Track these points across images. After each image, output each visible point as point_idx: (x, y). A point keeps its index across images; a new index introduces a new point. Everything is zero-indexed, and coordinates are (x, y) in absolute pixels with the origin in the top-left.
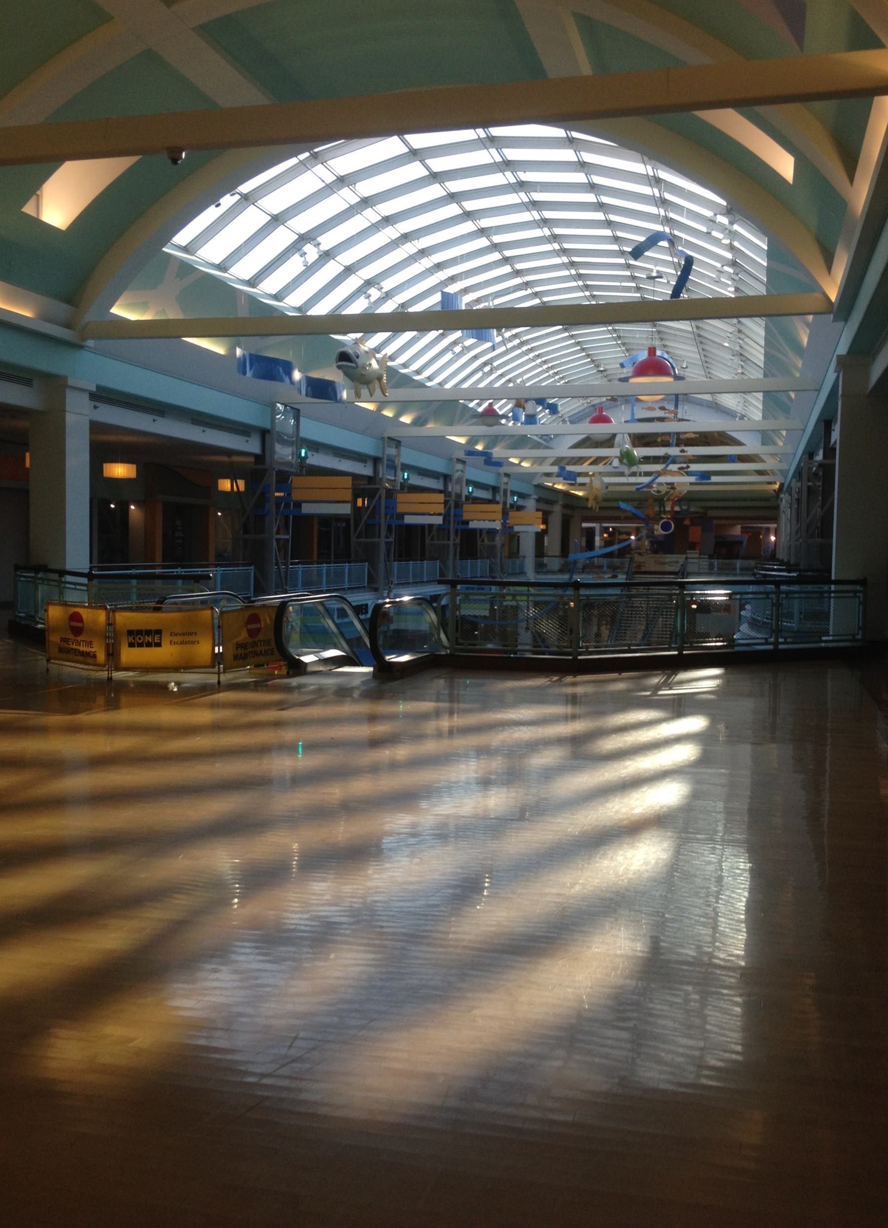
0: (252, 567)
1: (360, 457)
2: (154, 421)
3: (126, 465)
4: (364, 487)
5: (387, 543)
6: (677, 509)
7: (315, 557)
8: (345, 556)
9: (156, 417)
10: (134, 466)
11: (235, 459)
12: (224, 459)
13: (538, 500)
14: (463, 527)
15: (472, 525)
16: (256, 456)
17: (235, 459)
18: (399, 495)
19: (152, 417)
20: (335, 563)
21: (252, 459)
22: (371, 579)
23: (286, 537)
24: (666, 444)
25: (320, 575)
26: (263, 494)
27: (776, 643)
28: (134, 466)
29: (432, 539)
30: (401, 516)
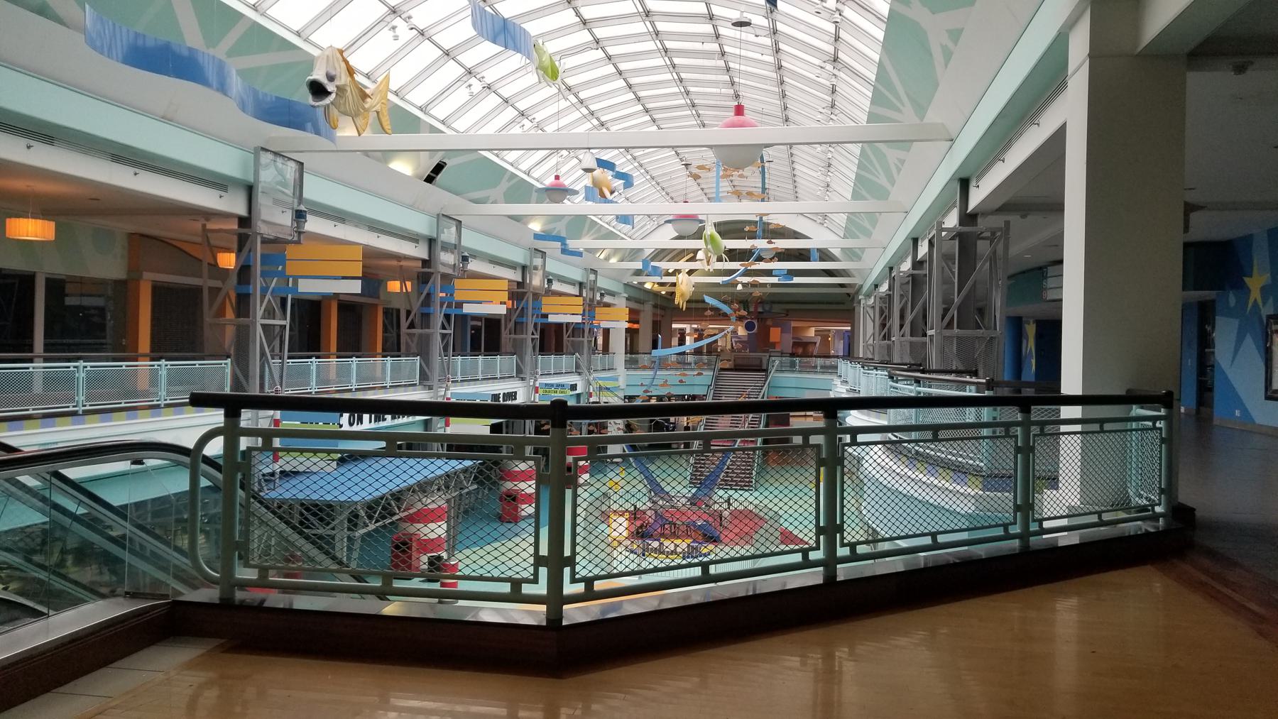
0: (229, 361)
1: (512, 266)
2: (29, 147)
3: (40, 222)
4: (424, 273)
5: (444, 336)
6: (760, 310)
7: (379, 350)
8: (559, 350)
9: (32, 143)
10: (53, 224)
11: (403, 263)
12: (394, 263)
13: (655, 306)
14: (544, 321)
15: (552, 319)
16: (518, 283)
17: (403, 263)
18: (456, 281)
19: (132, 170)
20: (46, 360)
21: (420, 264)
22: (519, 371)
23: (283, 323)
24: (752, 236)
25: (154, 380)
26: (429, 295)
27: (830, 562)
28: (53, 224)
29: (412, 326)
30: (546, 316)
